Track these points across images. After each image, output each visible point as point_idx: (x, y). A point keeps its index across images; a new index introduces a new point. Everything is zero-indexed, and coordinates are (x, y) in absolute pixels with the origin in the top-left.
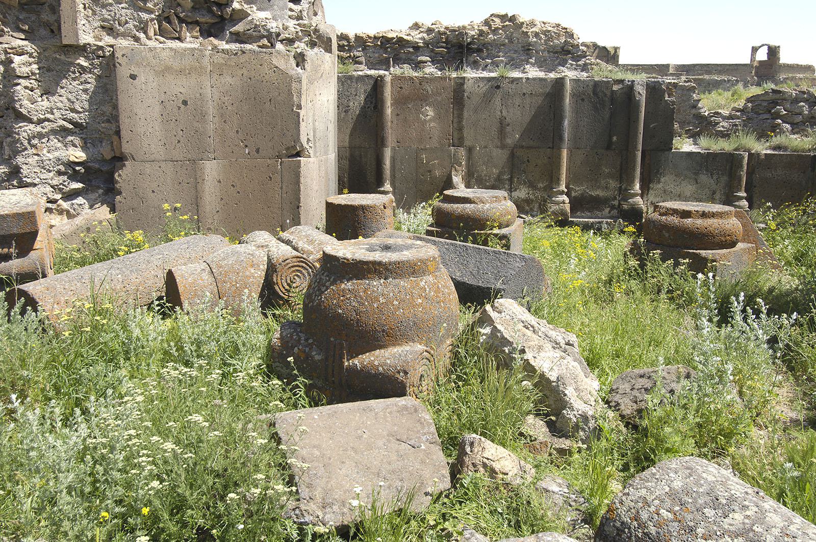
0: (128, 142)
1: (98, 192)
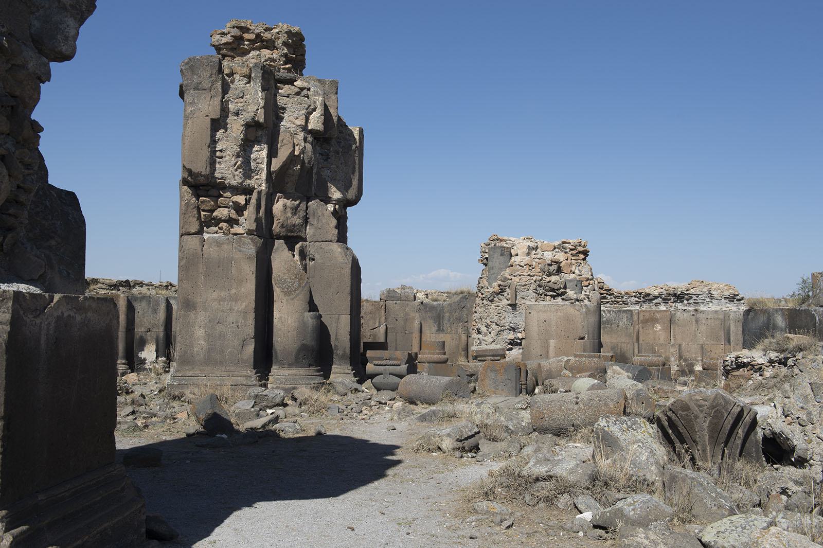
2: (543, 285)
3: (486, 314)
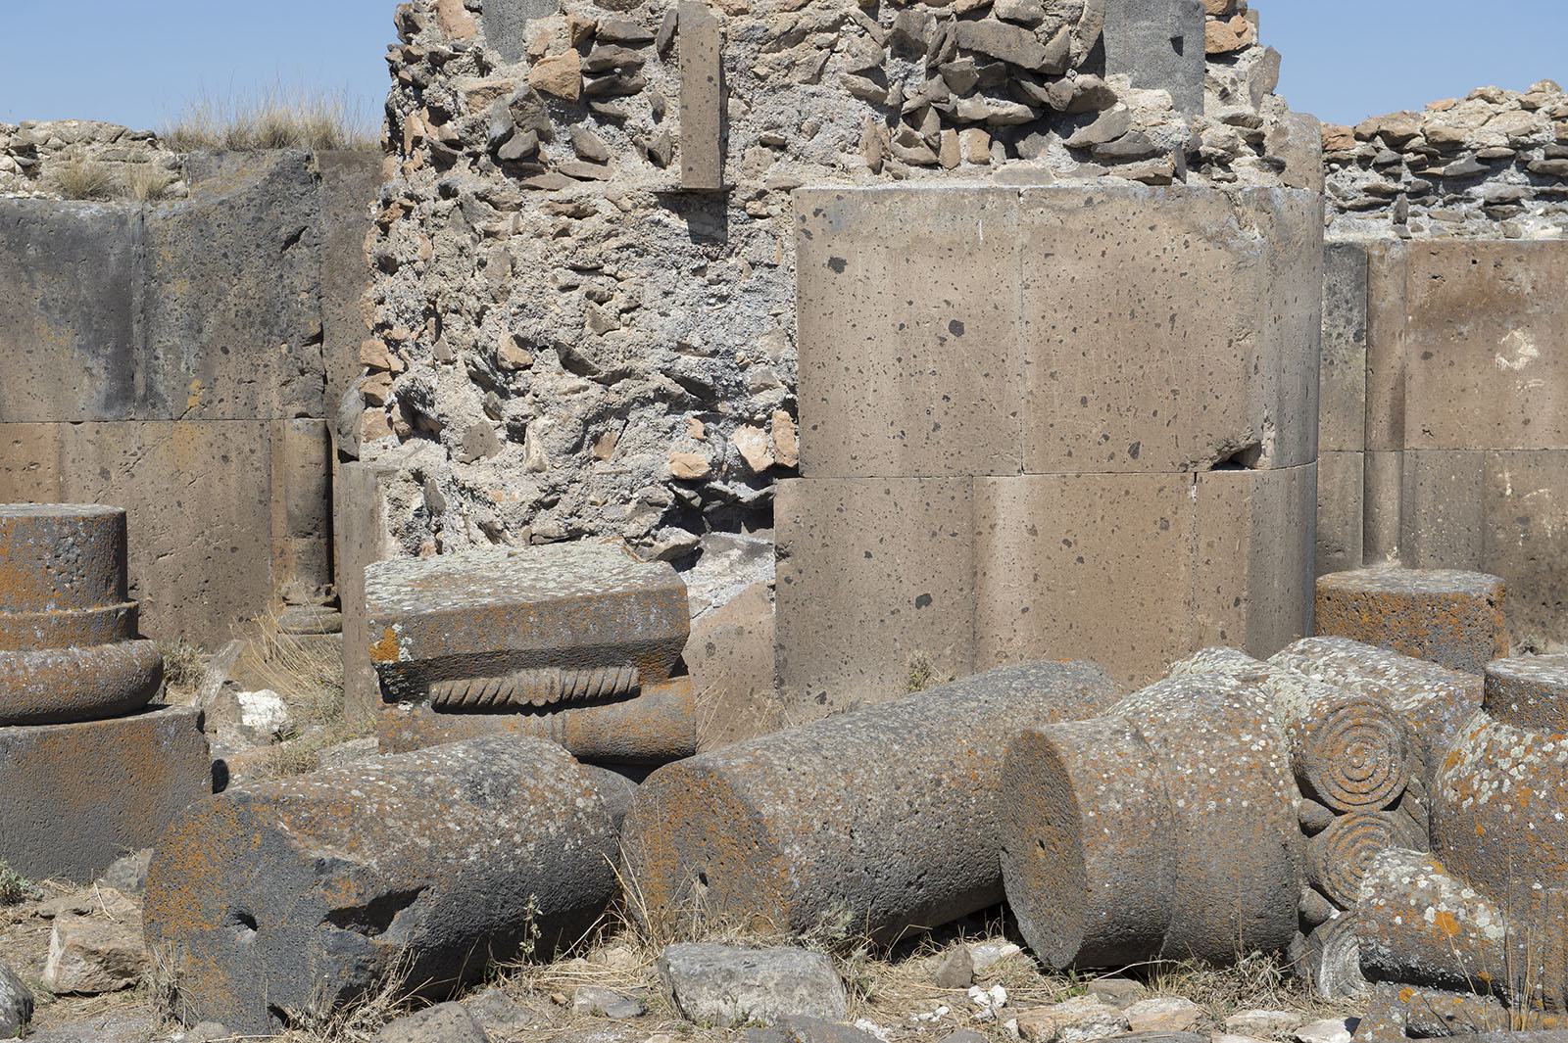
0: (815, 428)
1: (728, 556)
2: (930, 40)
3: (479, 280)
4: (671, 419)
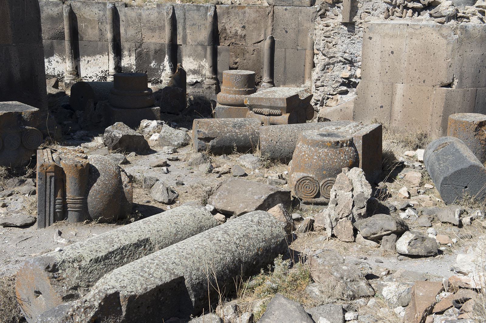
4: (343, 66)
